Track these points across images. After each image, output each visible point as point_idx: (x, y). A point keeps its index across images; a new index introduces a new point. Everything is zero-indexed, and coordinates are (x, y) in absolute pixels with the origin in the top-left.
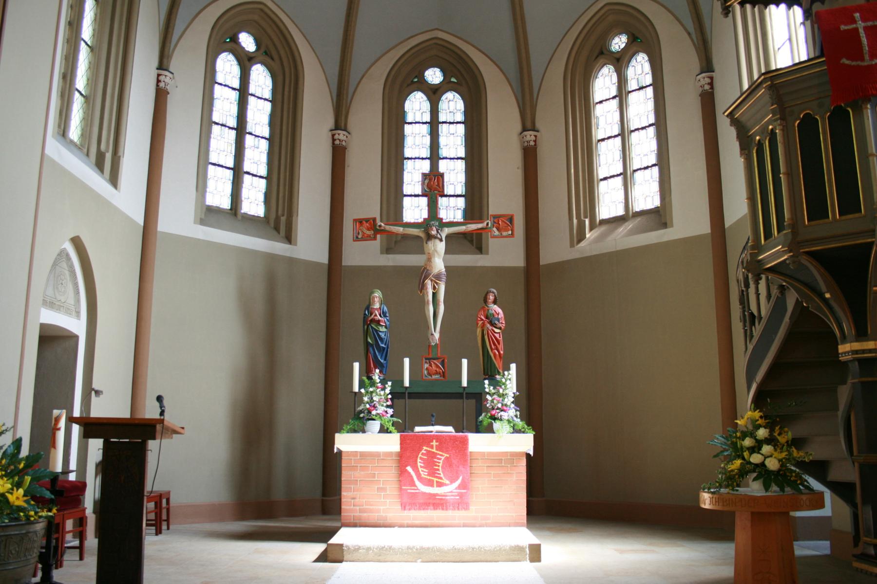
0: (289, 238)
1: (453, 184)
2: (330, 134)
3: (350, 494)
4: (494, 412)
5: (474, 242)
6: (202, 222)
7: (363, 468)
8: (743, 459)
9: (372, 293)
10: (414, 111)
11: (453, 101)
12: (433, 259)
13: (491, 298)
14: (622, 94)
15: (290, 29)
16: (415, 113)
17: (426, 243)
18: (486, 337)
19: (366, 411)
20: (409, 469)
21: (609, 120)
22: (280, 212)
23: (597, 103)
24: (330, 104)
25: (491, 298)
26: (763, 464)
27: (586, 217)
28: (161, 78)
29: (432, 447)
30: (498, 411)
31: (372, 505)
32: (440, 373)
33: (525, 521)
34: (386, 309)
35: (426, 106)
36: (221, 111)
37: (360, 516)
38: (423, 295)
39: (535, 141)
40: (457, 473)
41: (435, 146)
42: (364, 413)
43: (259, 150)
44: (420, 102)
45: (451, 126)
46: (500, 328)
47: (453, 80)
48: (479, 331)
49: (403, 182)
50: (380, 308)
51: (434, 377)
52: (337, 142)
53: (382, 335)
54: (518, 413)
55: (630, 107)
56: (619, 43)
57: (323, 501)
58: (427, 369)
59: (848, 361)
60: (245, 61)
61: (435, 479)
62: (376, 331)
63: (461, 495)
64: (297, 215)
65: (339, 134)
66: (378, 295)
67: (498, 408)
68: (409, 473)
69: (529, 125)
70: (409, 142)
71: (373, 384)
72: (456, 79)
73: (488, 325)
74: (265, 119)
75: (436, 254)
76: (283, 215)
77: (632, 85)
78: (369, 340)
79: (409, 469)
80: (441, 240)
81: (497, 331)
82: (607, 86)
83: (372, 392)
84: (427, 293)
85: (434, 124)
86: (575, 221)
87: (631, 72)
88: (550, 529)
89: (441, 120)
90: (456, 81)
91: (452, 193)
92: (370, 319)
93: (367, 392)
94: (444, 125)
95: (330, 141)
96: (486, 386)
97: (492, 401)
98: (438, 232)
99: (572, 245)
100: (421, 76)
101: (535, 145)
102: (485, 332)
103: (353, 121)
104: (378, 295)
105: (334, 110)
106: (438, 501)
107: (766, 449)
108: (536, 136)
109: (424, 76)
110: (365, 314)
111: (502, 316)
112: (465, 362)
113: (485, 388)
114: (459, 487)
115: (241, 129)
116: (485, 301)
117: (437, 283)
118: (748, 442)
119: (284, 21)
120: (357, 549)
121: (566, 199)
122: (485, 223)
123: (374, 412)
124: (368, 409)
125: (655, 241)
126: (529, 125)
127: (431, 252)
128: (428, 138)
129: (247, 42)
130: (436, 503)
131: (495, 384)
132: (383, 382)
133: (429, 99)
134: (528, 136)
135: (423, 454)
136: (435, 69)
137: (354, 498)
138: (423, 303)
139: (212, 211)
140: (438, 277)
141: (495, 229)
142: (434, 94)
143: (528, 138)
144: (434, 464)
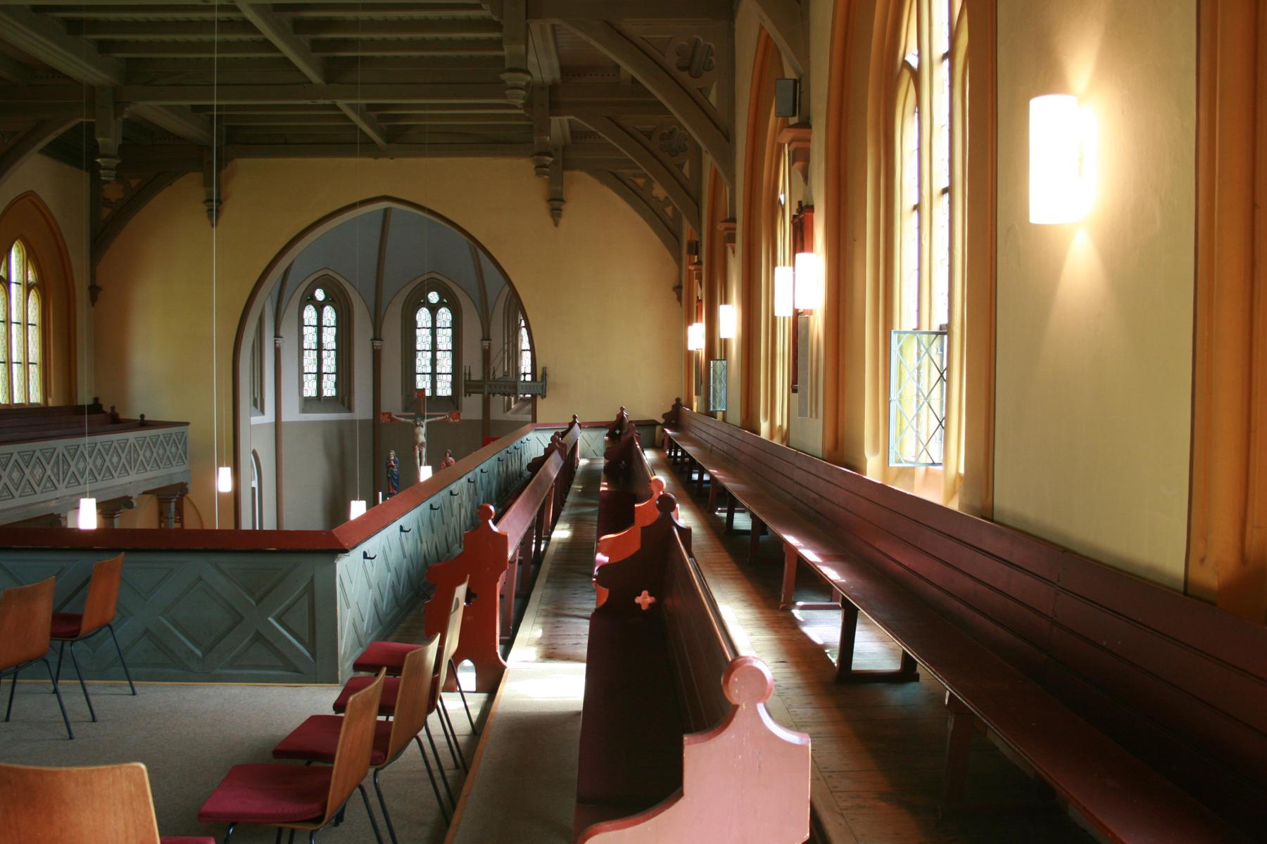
0: (350, 409)
2: (371, 342)
6: (303, 411)
25: (448, 454)
28: (277, 342)
34: (397, 459)
35: (429, 317)
39: (489, 346)
41: (434, 343)
45: (444, 330)
47: (445, 301)
52: (375, 347)
53: (396, 473)
60: (319, 308)
66: (392, 453)
69: (486, 337)
70: (419, 340)
74: (333, 339)
78: (389, 475)
80: (422, 426)
85: (434, 329)
89: (430, 352)
91: (444, 372)
99: (504, 412)
103: (385, 333)
104: (392, 453)
115: (320, 348)
128: (430, 337)
129: (320, 295)
138: (416, 458)
139: (308, 400)
140: (422, 445)
142: (434, 309)
143: (485, 344)
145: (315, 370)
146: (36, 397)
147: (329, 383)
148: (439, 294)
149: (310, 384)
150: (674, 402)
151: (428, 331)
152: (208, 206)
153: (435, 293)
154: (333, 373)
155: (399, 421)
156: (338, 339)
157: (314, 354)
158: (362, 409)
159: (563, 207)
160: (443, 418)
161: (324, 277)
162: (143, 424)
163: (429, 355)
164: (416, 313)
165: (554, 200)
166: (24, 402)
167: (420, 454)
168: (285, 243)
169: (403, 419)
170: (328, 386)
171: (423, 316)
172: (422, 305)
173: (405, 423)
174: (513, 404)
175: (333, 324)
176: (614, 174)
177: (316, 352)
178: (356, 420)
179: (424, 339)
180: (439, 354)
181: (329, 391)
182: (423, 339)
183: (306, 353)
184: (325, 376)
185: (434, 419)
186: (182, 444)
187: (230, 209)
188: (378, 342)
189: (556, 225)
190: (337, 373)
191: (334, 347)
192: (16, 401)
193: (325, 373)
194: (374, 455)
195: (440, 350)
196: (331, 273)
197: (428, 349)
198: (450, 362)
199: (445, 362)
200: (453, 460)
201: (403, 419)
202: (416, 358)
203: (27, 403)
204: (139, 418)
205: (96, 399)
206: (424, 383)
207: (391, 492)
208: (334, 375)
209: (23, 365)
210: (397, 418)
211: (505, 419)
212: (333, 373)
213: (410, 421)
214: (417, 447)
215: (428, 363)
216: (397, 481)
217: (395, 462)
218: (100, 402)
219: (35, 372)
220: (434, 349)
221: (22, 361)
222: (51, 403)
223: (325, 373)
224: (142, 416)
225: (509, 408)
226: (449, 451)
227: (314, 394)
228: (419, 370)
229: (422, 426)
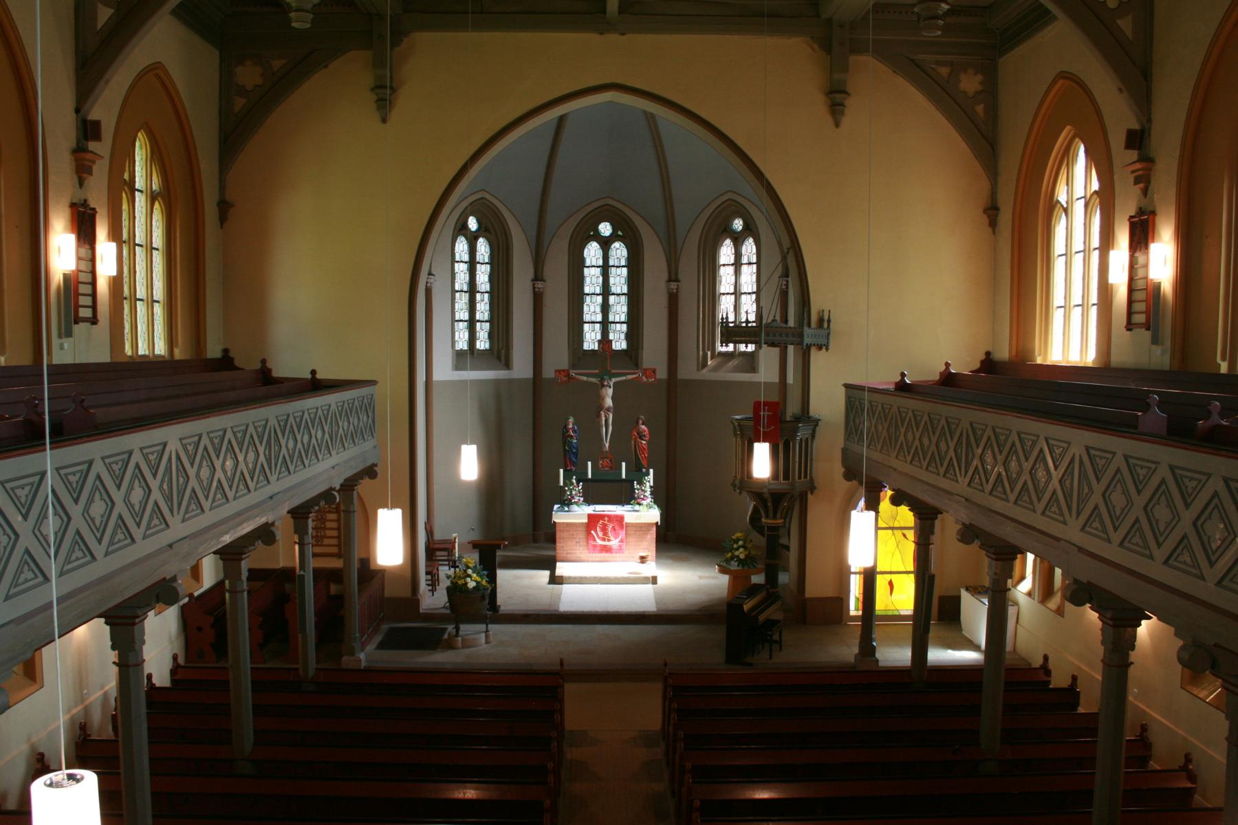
0: (507, 365)
2: (531, 283)
3: (561, 545)
9: (569, 419)
10: (591, 257)
13: (641, 422)
20: (593, 532)
22: (500, 347)
24: (531, 259)
25: (641, 422)
27: (709, 350)
33: (654, 559)
34: (576, 428)
35: (600, 253)
39: (677, 289)
47: (620, 233)
48: (633, 442)
49: (583, 313)
52: (537, 290)
56: (738, 224)
57: (533, 535)
59: (1148, 255)
63: (620, 546)
66: (571, 420)
69: (673, 277)
72: (622, 233)
74: (486, 278)
76: (503, 349)
77: (745, 260)
78: (567, 448)
79: (593, 532)
80: (610, 387)
81: (644, 442)
82: (728, 254)
85: (605, 269)
86: (701, 353)
87: (744, 248)
99: (698, 370)
103: (548, 271)
104: (571, 420)
107: (741, 550)
108: (678, 285)
116: (637, 423)
118: (735, 546)
120: (570, 578)
123: (573, 501)
125: (748, 380)
126: (673, 277)
129: (473, 224)
130: (606, 549)
131: (641, 483)
132: (578, 484)
133: (602, 247)
139: (459, 354)
140: (608, 409)
141: (644, 377)
142: (605, 244)
143: (672, 287)
144: (606, 530)
146: (161, 348)
148: (612, 224)
150: (983, 357)
152: (377, 94)
154: (486, 321)
155: (578, 379)
158: (521, 367)
159: (846, 102)
160: (634, 376)
162: (315, 385)
163: (599, 299)
165: (831, 92)
166: (147, 353)
167: (606, 421)
168: (479, 145)
170: (481, 338)
171: (592, 252)
172: (589, 239)
174: (709, 359)
175: (487, 261)
176: (912, 60)
177: (467, 295)
178: (761, 383)
179: (594, 280)
180: (612, 299)
181: (483, 343)
182: (592, 280)
184: (478, 324)
185: (624, 378)
186: (899, 443)
187: (405, 103)
188: (539, 283)
189: (837, 125)
190: (490, 321)
192: (141, 352)
193: (478, 321)
194: (534, 423)
195: (613, 294)
198: (625, 309)
199: (619, 308)
202: (583, 303)
203: (151, 355)
204: (309, 376)
205: (226, 351)
206: (593, 334)
207: (568, 468)
208: (488, 324)
209: (129, 300)
210: (577, 376)
212: (486, 321)
213: (593, 380)
214: (602, 413)
215: (598, 309)
216: (576, 454)
217: (574, 431)
219: (158, 310)
220: (606, 292)
221: (145, 298)
222: (178, 354)
223: (478, 321)
224: (313, 372)
225: (705, 365)
226: (642, 417)
227: (466, 347)
228: (587, 318)
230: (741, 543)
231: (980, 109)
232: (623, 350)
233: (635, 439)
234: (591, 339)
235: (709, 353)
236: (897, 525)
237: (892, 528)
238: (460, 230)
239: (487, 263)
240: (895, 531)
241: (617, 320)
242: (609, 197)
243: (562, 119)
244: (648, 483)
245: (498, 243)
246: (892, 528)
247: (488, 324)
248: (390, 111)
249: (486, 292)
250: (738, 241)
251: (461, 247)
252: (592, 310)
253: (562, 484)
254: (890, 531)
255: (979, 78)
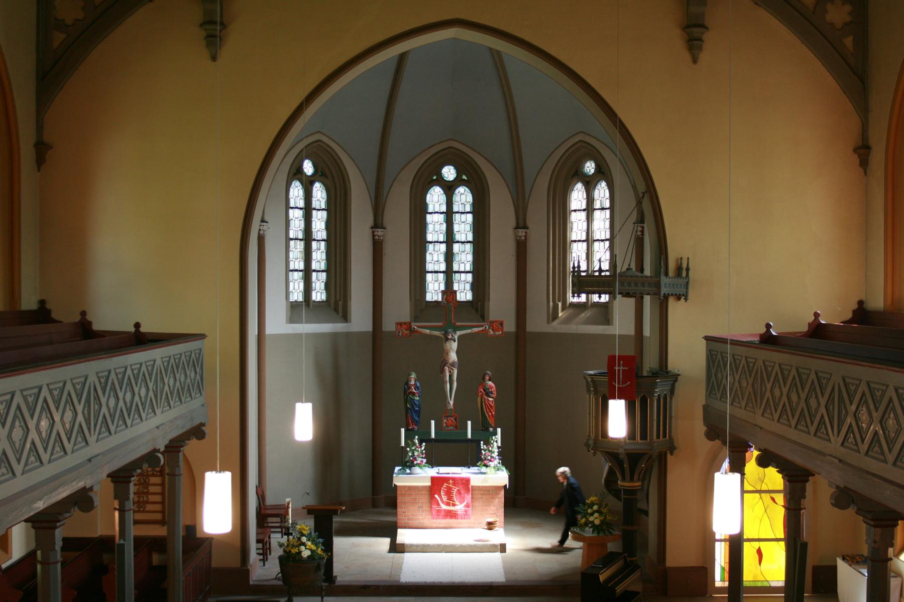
0: (345, 318)
1: (463, 263)
3: (402, 510)
4: (486, 462)
5: (479, 310)
7: (410, 495)
8: (587, 518)
11: (464, 194)
12: (449, 354)
13: (487, 378)
14: (590, 210)
15: (339, 155)
16: (434, 205)
17: (445, 343)
18: (484, 404)
19: (410, 462)
20: (436, 496)
21: (580, 228)
23: (572, 211)
25: (487, 378)
26: (593, 522)
27: (559, 301)
29: (449, 484)
30: (488, 461)
31: (414, 516)
32: (454, 426)
35: (443, 198)
36: (294, 229)
37: (408, 522)
38: (443, 377)
39: (525, 236)
40: (464, 498)
42: (409, 462)
43: (321, 251)
44: (439, 195)
45: (462, 215)
46: (493, 398)
47: (464, 177)
48: (479, 399)
50: (415, 384)
51: (450, 428)
52: (376, 238)
53: (417, 403)
54: (501, 461)
55: (595, 221)
56: (590, 167)
58: (445, 423)
61: (451, 502)
62: (413, 400)
63: (466, 511)
64: (351, 300)
65: (378, 231)
66: (413, 376)
67: (488, 460)
68: (436, 499)
69: (521, 224)
70: (430, 228)
71: (414, 444)
72: (467, 177)
73: (485, 396)
74: (323, 225)
75: (451, 351)
76: (340, 301)
77: (597, 205)
78: (408, 406)
79: (436, 496)
80: (455, 341)
83: (413, 450)
84: (446, 375)
85: (449, 215)
86: (551, 304)
87: (596, 193)
88: (523, 524)
90: (466, 178)
92: (409, 391)
93: (411, 449)
94: (457, 214)
95: (371, 235)
96: (482, 445)
97: (485, 454)
98: (452, 336)
99: (548, 322)
100: (440, 175)
101: (526, 239)
102: (483, 400)
104: (413, 376)
105: (373, 209)
106: (453, 514)
107: (596, 515)
108: (526, 232)
109: (441, 173)
110: (405, 388)
111: (495, 389)
112: (469, 423)
113: (481, 446)
114: (465, 506)
116: (484, 378)
117: (452, 369)
118: (589, 511)
119: (330, 145)
120: (411, 546)
121: (546, 292)
122: (484, 327)
123: (415, 462)
124: (412, 460)
126: (521, 224)
127: (448, 349)
128: (445, 225)
129: (308, 168)
130: (451, 515)
131: (487, 443)
132: (420, 444)
133: (445, 193)
134: (520, 233)
135: (444, 488)
136: (450, 167)
137: (404, 512)
138: (444, 382)
139: (294, 306)
140: (453, 365)
141: (490, 330)
142: (449, 189)
143: (520, 234)
145: (302, 267)
147: (318, 284)
148: (455, 168)
149: (296, 284)
150: (856, 306)
151: (442, 216)
152: (206, 30)
153: (452, 168)
154: (323, 271)
155: (421, 333)
156: (329, 225)
157: (300, 245)
159: (704, 37)
160: (481, 329)
161: (316, 144)
163: (443, 247)
164: (427, 193)
167: (451, 376)
169: (428, 331)
170: (318, 288)
171: (435, 198)
173: (431, 336)
177: (302, 243)
180: (456, 247)
181: (319, 294)
183: (292, 243)
184: (314, 274)
185: (469, 331)
188: (380, 230)
191: (325, 237)
195: (458, 242)
196: (325, 139)
197: (442, 240)
198: (470, 257)
200: (493, 385)
201: (428, 331)
204: (133, 330)
205: (42, 302)
206: (436, 284)
210: (419, 329)
211: (552, 331)
212: (323, 271)
214: (446, 368)
216: (418, 413)
217: (416, 388)
218: (48, 306)
220: (450, 240)
223: (314, 271)
224: (137, 325)
225: (555, 316)
227: (301, 299)
229: (455, 341)
230: (595, 507)
231: (849, 41)
232: (468, 302)
233: (482, 395)
234: (434, 289)
235: (560, 304)
236: (764, 488)
237: (760, 492)
238: (295, 174)
239: (323, 210)
240: (763, 495)
241: (462, 269)
242: (319, 132)
243: (402, 57)
244: (495, 443)
245: (336, 188)
246: (760, 492)
247: (324, 274)
248: (220, 48)
249: (323, 240)
250: (590, 185)
251: (296, 192)
252: (435, 259)
253: (403, 444)
254: (757, 495)
255: (848, 8)
